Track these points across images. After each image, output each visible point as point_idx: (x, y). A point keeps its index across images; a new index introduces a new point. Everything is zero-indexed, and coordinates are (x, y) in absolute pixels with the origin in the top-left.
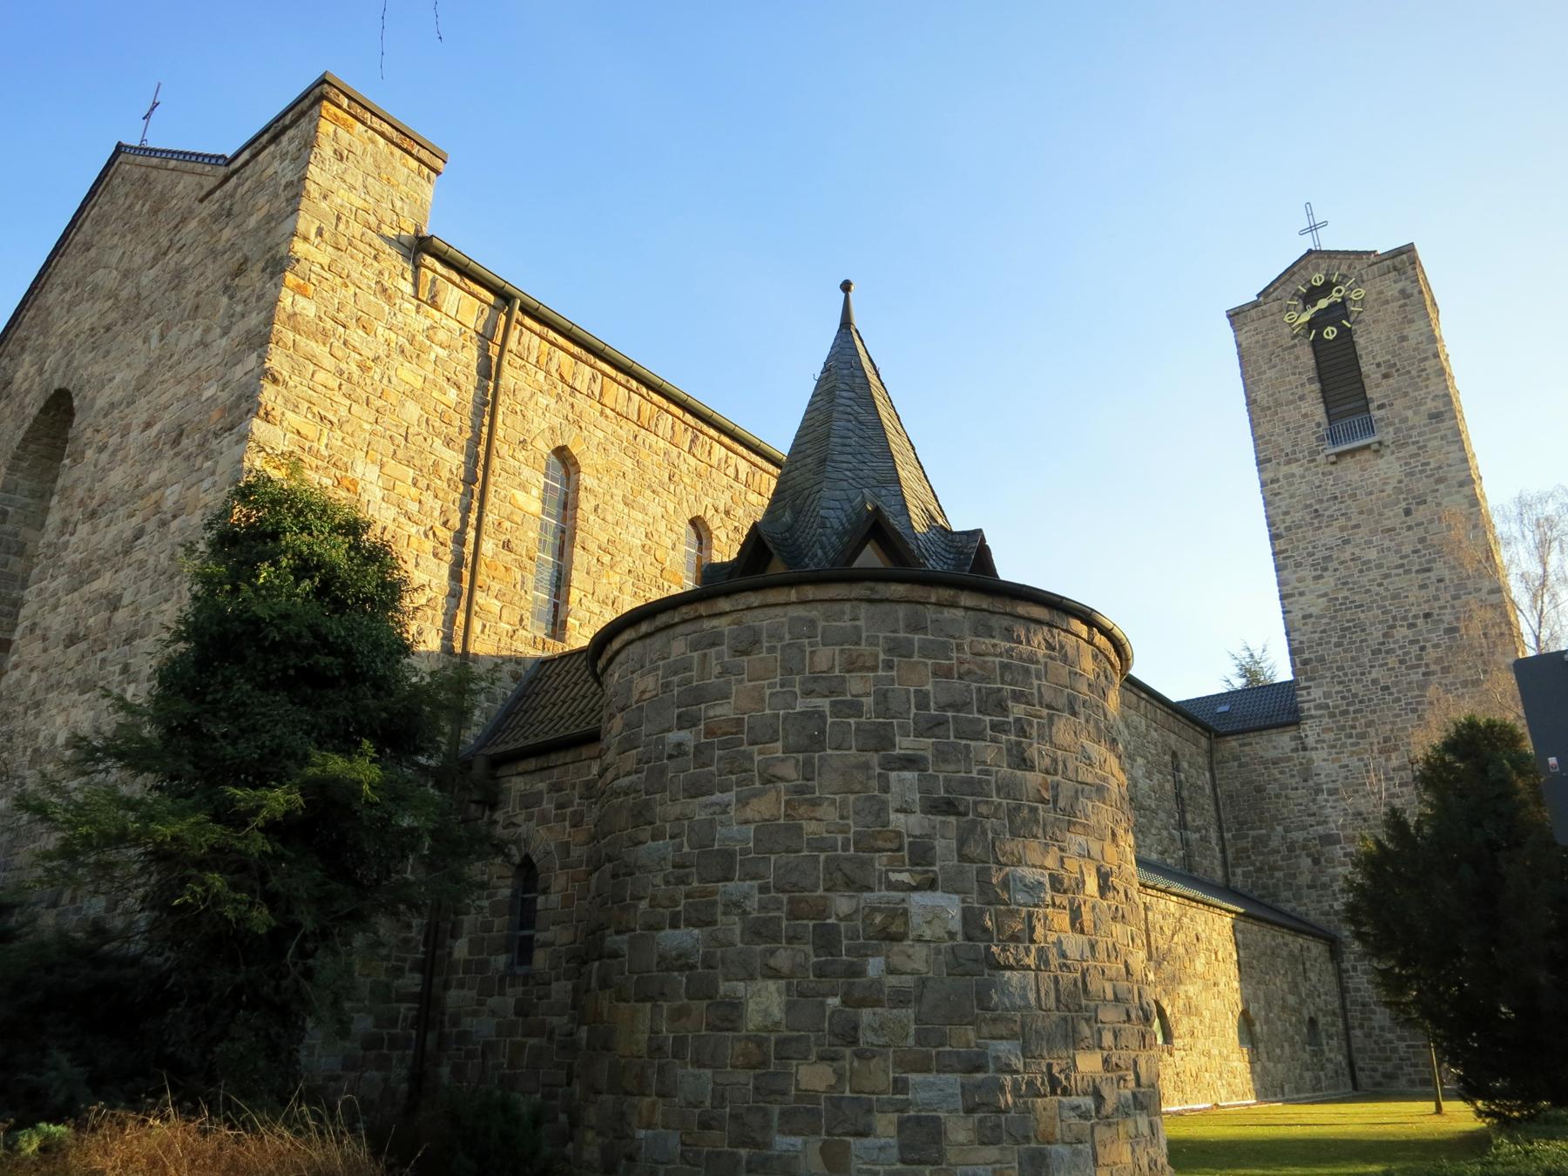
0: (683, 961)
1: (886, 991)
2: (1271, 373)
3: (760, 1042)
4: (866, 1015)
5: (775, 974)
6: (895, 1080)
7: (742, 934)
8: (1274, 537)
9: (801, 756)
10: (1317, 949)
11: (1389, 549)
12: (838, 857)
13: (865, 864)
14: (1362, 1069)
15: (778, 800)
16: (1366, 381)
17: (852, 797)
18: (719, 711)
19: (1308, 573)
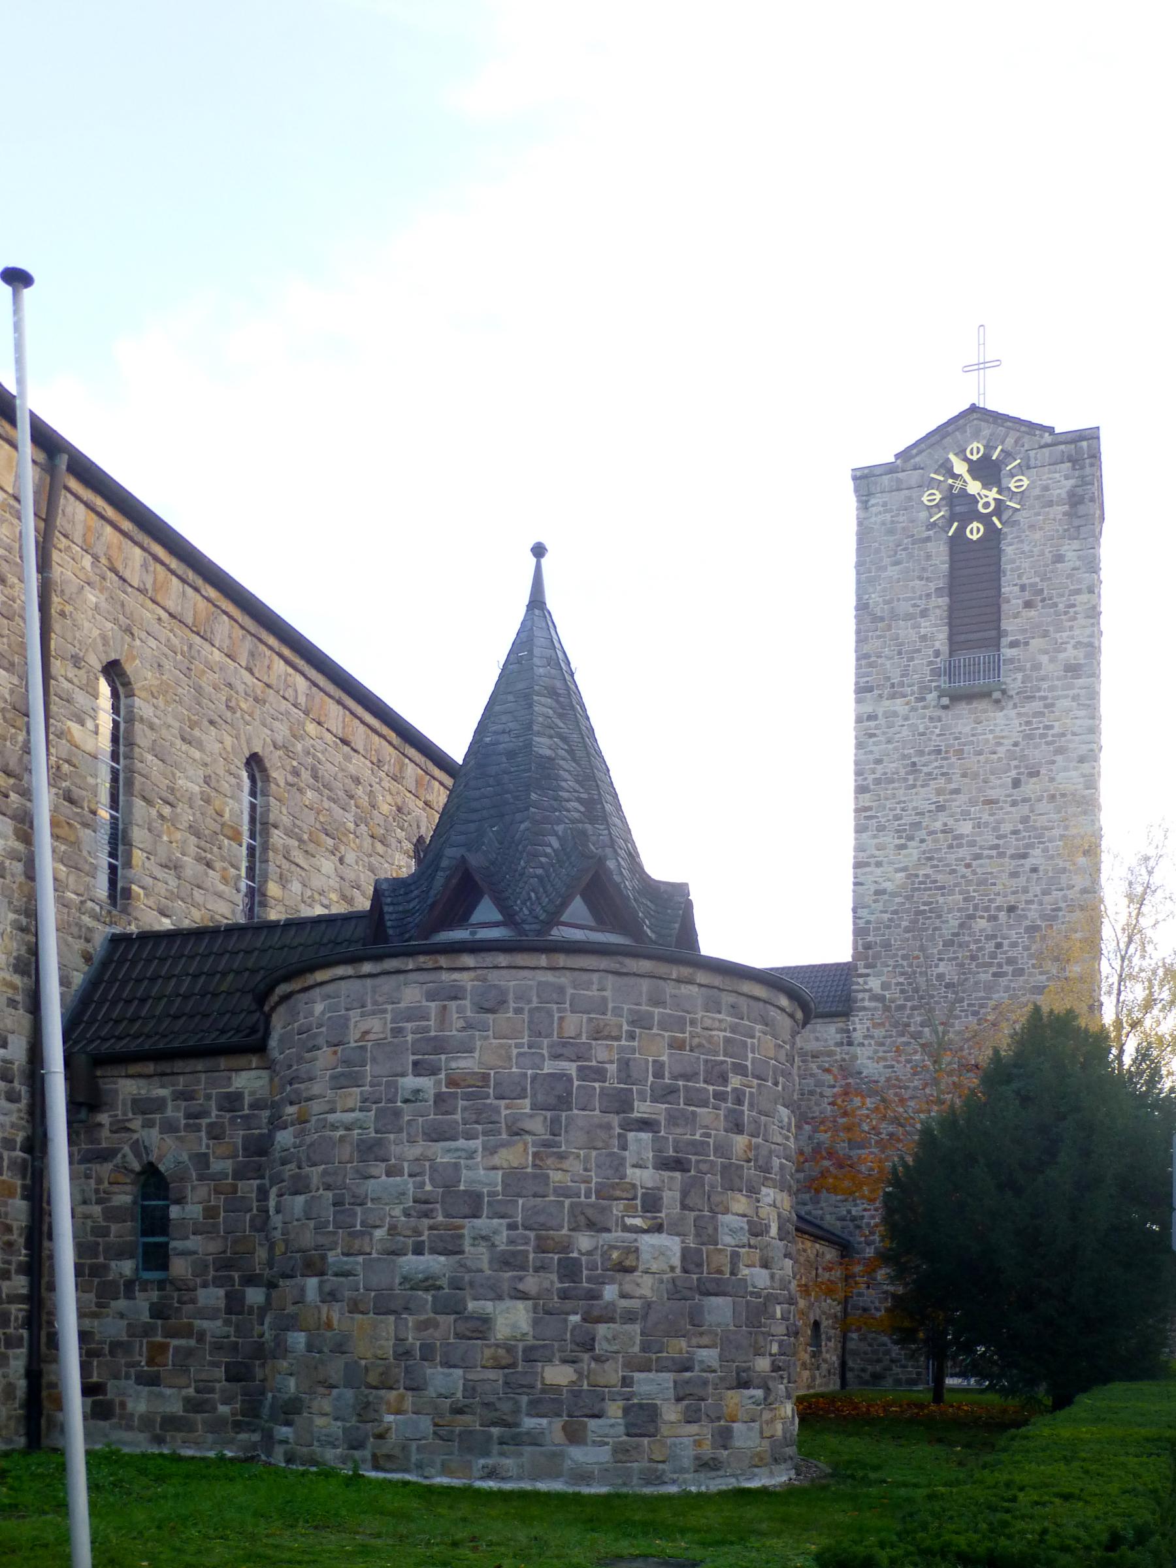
0: (430, 1282)
1: (619, 1311)
2: (893, 572)
3: (510, 1350)
4: (602, 1329)
5: (523, 1296)
6: (624, 1378)
7: (490, 1262)
8: (861, 790)
9: (549, 1114)
10: (830, 1254)
11: (986, 824)
12: (580, 1204)
13: (603, 1210)
14: (852, 1370)
15: (525, 1150)
16: (1004, 607)
17: (594, 1153)
18: (462, 1064)
19: (890, 840)
